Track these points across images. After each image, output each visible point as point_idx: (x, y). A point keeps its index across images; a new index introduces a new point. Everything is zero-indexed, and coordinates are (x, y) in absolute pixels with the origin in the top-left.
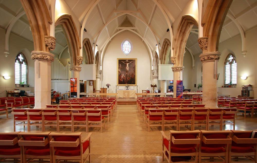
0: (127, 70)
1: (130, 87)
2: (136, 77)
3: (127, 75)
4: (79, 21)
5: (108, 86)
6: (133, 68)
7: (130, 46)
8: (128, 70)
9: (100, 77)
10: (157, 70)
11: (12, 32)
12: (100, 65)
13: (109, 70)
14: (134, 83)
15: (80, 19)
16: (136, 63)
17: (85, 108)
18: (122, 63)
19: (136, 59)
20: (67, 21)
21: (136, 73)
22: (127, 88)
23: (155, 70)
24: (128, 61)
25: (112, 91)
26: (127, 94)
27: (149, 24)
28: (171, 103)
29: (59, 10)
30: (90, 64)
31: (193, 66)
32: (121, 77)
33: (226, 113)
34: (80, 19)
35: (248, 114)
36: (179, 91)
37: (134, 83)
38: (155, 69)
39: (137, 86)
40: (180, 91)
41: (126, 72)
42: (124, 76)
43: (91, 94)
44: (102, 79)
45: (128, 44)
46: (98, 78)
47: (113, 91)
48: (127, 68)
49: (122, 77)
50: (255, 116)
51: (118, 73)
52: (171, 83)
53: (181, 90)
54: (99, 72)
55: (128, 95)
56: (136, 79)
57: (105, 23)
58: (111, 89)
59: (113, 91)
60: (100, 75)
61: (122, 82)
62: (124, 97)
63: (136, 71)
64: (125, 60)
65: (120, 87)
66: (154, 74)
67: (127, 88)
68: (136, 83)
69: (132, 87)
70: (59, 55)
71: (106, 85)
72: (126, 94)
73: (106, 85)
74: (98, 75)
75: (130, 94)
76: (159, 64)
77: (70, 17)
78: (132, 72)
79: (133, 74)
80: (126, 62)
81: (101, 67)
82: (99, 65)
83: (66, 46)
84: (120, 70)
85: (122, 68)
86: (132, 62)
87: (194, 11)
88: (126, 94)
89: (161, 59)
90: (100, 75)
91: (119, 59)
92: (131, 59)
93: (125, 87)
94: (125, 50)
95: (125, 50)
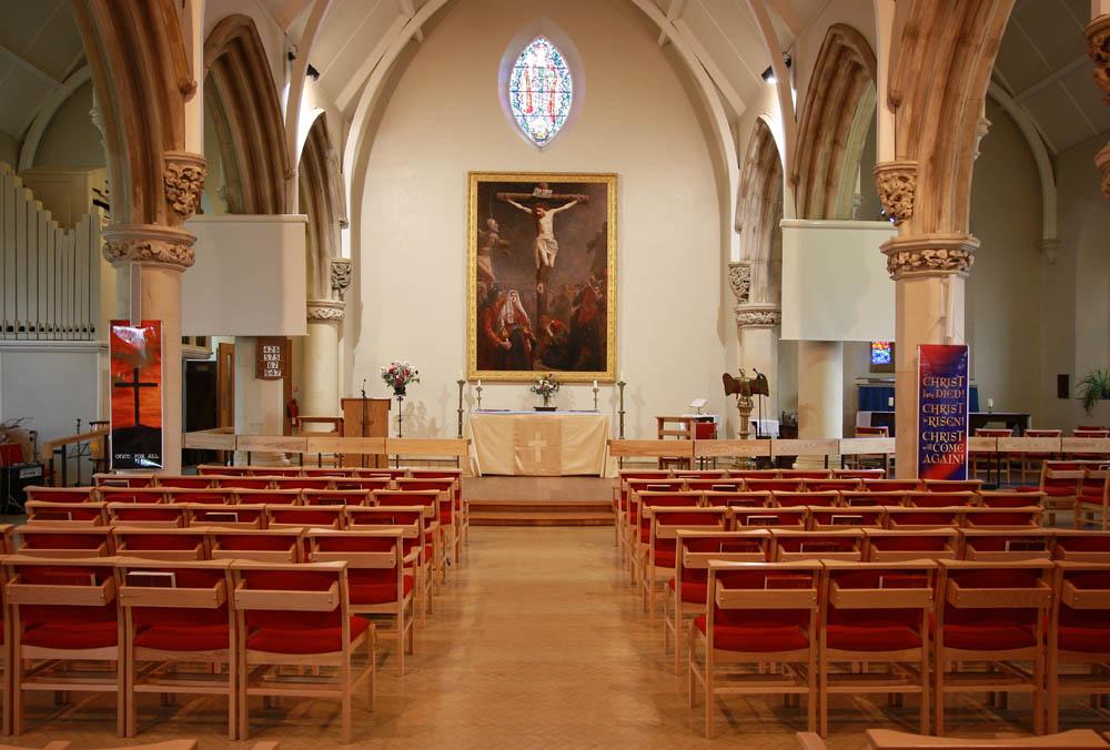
0: (542, 262)
2: (610, 318)
5: (399, 381)
6: (591, 245)
7: (562, 82)
8: (550, 262)
9: (339, 313)
16: (611, 211)
18: (505, 207)
19: (614, 176)
21: (610, 288)
22: (539, 401)
23: (759, 260)
24: (547, 193)
31: (1050, 232)
32: (495, 315)
36: (939, 429)
38: (753, 256)
39: (622, 385)
40: (947, 429)
42: (517, 310)
44: (350, 327)
46: (321, 320)
47: (433, 421)
48: (547, 246)
49: (507, 312)
51: (474, 282)
52: (880, 360)
54: (329, 273)
55: (553, 451)
58: (421, 406)
59: (433, 421)
60: (337, 300)
62: (523, 470)
63: (611, 272)
64: (530, 187)
67: (546, 399)
68: (610, 360)
69: (578, 395)
72: (537, 444)
75: (569, 443)
78: (585, 275)
79: (586, 294)
80: (534, 202)
82: (331, 221)
84: (487, 261)
85: (503, 246)
86: (582, 200)
88: (537, 444)
89: (803, 180)
90: (341, 296)
93: (525, 389)
95: (524, 107)
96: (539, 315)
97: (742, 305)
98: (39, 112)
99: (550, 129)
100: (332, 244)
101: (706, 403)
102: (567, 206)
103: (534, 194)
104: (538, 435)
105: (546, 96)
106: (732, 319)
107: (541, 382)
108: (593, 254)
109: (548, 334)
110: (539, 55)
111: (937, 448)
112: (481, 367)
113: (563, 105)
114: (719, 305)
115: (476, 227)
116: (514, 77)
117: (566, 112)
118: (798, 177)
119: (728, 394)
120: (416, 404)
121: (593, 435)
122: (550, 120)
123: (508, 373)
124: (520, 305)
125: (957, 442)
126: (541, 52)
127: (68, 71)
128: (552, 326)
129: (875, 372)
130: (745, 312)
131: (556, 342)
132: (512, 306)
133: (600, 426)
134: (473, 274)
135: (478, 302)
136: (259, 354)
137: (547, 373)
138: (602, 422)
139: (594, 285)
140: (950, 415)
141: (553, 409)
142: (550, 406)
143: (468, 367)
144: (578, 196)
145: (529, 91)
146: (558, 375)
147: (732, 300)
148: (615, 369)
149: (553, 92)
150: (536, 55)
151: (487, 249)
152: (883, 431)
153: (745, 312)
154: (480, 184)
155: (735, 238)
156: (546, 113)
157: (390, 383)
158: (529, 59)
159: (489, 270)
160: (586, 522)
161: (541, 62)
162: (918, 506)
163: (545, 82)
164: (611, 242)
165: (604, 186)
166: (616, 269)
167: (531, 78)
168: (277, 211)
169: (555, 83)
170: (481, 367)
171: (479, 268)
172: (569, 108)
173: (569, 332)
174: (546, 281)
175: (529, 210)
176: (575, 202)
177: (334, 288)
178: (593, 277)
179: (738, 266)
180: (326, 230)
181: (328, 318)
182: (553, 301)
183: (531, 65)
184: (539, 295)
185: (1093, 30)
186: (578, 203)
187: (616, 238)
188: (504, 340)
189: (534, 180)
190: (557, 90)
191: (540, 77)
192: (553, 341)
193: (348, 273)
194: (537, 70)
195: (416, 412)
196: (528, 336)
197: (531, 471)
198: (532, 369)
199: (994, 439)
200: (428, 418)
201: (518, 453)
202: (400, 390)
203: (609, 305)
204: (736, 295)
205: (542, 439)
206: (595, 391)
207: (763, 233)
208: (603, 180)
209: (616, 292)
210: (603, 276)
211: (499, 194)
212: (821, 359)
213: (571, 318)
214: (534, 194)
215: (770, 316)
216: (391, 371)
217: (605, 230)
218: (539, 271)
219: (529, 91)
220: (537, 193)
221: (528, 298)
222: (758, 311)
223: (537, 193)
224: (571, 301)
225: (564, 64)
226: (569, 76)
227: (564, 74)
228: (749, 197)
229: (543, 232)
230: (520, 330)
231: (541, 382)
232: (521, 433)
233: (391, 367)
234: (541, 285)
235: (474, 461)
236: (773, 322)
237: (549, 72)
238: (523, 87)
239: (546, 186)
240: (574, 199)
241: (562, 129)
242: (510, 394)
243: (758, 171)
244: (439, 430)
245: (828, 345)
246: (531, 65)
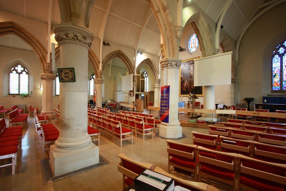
0: (191, 75)
11: (112, 66)
17: (225, 126)
28: (262, 123)
32: (183, 85)
33: (118, 127)
36: (164, 106)
42: (187, 84)
49: (185, 85)
50: (2, 108)
53: (167, 103)
60: (158, 85)
61: (184, 91)
65: (183, 98)
70: (236, 42)
74: (156, 84)
76: (25, 109)
77: (148, 59)
82: (156, 73)
94: (192, 47)
95: (191, 47)
111: (163, 111)
112: (181, 94)
123: (200, 95)
124: (187, 83)
125: (167, 110)
129: (273, 93)
140: (166, 103)
152: (268, 111)
158: (192, 38)
162: (114, 120)
170: (181, 94)
199: (258, 112)
221: (188, 81)
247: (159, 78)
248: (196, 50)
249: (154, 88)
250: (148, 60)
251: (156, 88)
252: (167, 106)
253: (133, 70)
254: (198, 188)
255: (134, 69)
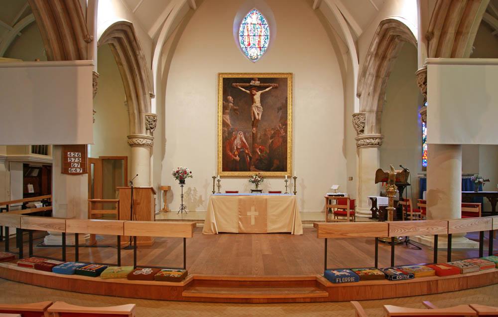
0: (255, 118)
1: (265, 180)
2: (289, 145)
3: (254, 136)
4: (150, 38)
5: (181, 176)
6: (279, 109)
7: (264, 31)
8: (259, 117)
9: (149, 142)
10: (377, 112)
12: (148, 96)
13: (190, 117)
14: (283, 168)
15: (152, 33)
16: (289, 92)
18: (236, 90)
19: (291, 74)
20: (122, 36)
21: (289, 129)
22: (253, 187)
23: (371, 111)
24: (257, 83)
25: (197, 198)
26: (257, 213)
27: (314, 7)
29: (108, 12)
30: (65, 57)
34: (152, 33)
35: (408, 213)
37: (283, 168)
38: (368, 109)
39: (295, 178)
41: (253, 125)
42: (242, 141)
43: (40, 225)
44: (159, 150)
45: (260, 22)
47: (201, 197)
48: (257, 109)
49: (237, 142)
51: (221, 127)
54: (144, 121)
55: (263, 217)
56: (289, 151)
57: (194, 6)
58: (195, 190)
59: (201, 197)
60: (149, 135)
61: (235, 160)
62: (244, 230)
63: (289, 122)
64: (249, 80)
66: (362, 131)
67: (257, 185)
68: (289, 166)
69: (273, 182)
71: (175, 174)
72: (252, 214)
73: (175, 174)
74: (141, 132)
75: (272, 213)
77: (130, 26)
78: (277, 124)
79: (277, 133)
80: (250, 88)
81: (154, 101)
82: (144, 94)
83: (18, 21)
84: (228, 117)
85: (235, 110)
86: (275, 87)
87: (407, 11)
88: (252, 214)
89: (437, 33)
90: (152, 133)
91: (226, 76)
92: (275, 76)
93: (246, 181)
94: (249, 44)
95: (246, 43)
96: (253, 144)
97: (360, 135)
98: (332, 233)
99: (259, 54)
100: (146, 106)
101: (339, 187)
102: (267, 90)
103: (251, 84)
104: (253, 208)
105: (257, 38)
106: (353, 144)
107: (254, 177)
108: (280, 113)
109: (258, 153)
110: (253, 18)
113: (265, 42)
114: (343, 138)
115: (222, 100)
116: (241, 29)
117: (266, 45)
118: (433, 33)
119: (376, 183)
120: (193, 188)
121: (285, 209)
122: (258, 49)
126: (254, 16)
127: (15, 21)
128: (260, 149)
130: (362, 139)
131: (262, 157)
132: (240, 139)
133: (291, 202)
134: (221, 123)
135: (223, 137)
136: (65, 158)
137: (257, 173)
138: (292, 199)
139: (281, 128)
141: (260, 191)
142: (259, 189)
143: (218, 170)
144: (273, 84)
145: (248, 35)
146: (263, 173)
147: (353, 133)
148: (291, 171)
149: (260, 36)
150: (252, 18)
151: (227, 111)
153: (362, 139)
154: (224, 79)
155: (357, 100)
156: (257, 46)
157: (177, 178)
158: (249, 20)
159: (229, 122)
160: (297, 301)
161: (255, 22)
163: (256, 31)
164: (289, 107)
165: (286, 79)
166: (292, 120)
167: (249, 29)
168: (80, 57)
169: (261, 32)
171: (223, 120)
172: (268, 43)
173: (268, 152)
174: (257, 127)
175: (248, 91)
176: (271, 87)
177: (147, 129)
178: (280, 125)
179: (358, 115)
180: (141, 98)
181: (143, 144)
182: (260, 137)
183: (249, 23)
184: (253, 133)
185: (418, 73)
186: (273, 88)
187: (292, 105)
188: (236, 157)
189: (251, 76)
190: (262, 34)
191: (254, 29)
192: (260, 157)
193: (155, 121)
194: (252, 25)
195: (192, 192)
196: (248, 154)
197: (249, 230)
198: (250, 171)
200: (198, 195)
201: (240, 219)
202: (182, 182)
203: (288, 138)
204: (357, 130)
205: (255, 211)
206: (286, 181)
207: (374, 96)
208: (285, 76)
209: (292, 132)
210: (285, 124)
211: (233, 84)
212: (450, 158)
213: (270, 145)
214: (251, 84)
215: (377, 141)
216: (178, 172)
217: (286, 101)
218: (253, 122)
219: (248, 35)
220: (252, 83)
222: (370, 138)
223: (252, 83)
224: (269, 136)
225: (266, 22)
226: (268, 28)
227: (266, 27)
228: (367, 76)
229: (255, 103)
230: (244, 151)
231: (254, 177)
232: (243, 207)
233: (178, 170)
234: (255, 129)
235: (213, 223)
236: (378, 144)
237: (257, 26)
238: (246, 34)
239: (257, 79)
240: (271, 86)
241: (264, 54)
242: (240, 183)
243: (375, 60)
244: (204, 201)
245: (455, 147)
246: (249, 23)
247: (154, 110)
248: (262, 56)
249: (133, 145)
250: (386, 26)
251: (143, 145)
252: (31, 236)
253: (83, 44)
254: (487, 313)
255: (89, 41)
